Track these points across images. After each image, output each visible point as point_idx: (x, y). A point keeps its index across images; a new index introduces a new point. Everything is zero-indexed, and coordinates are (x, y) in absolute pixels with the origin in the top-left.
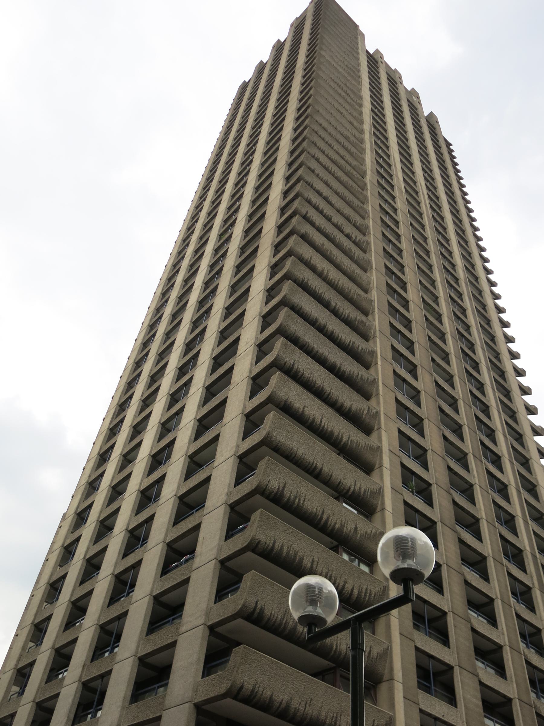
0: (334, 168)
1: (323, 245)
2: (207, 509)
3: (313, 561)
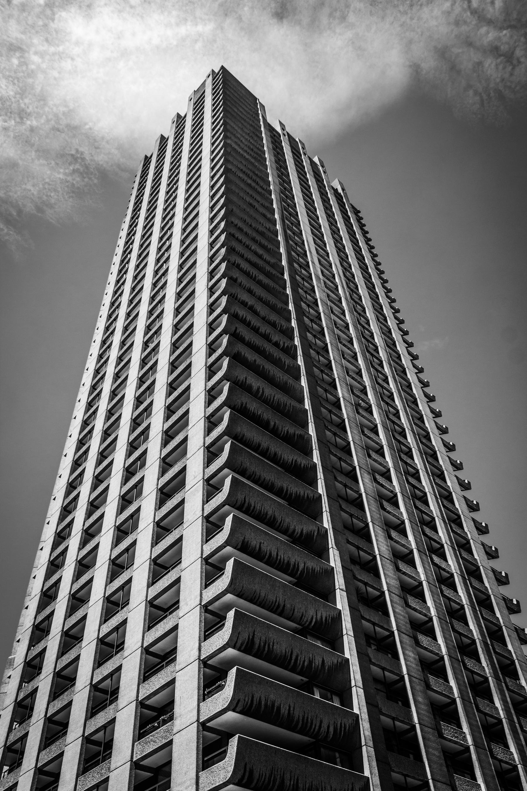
0: (254, 272)
1: (255, 361)
2: (179, 665)
3: (290, 707)
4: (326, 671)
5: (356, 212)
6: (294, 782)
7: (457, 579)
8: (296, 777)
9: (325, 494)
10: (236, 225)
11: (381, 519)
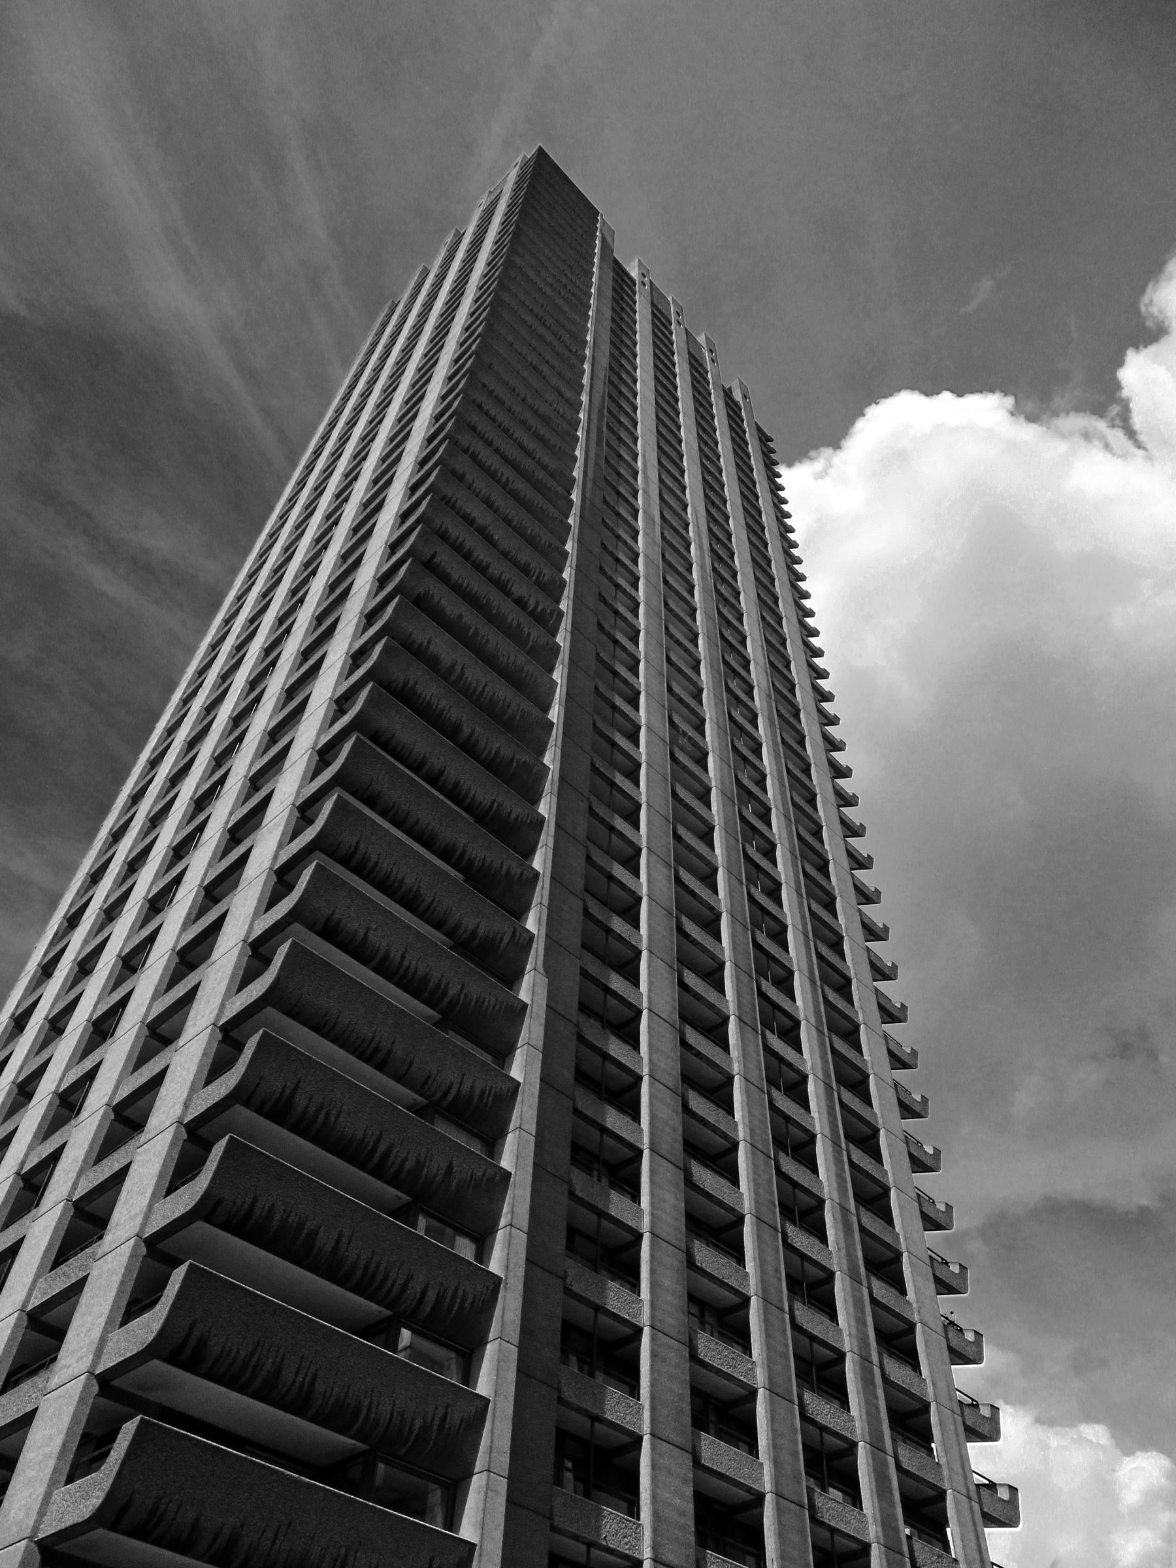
1: (460, 616)
4: (453, 1188)
5: (764, 439)
6: (304, 1378)
7: (813, 1089)
8: (312, 1370)
9: (548, 874)
10: (491, 392)
11: (672, 950)
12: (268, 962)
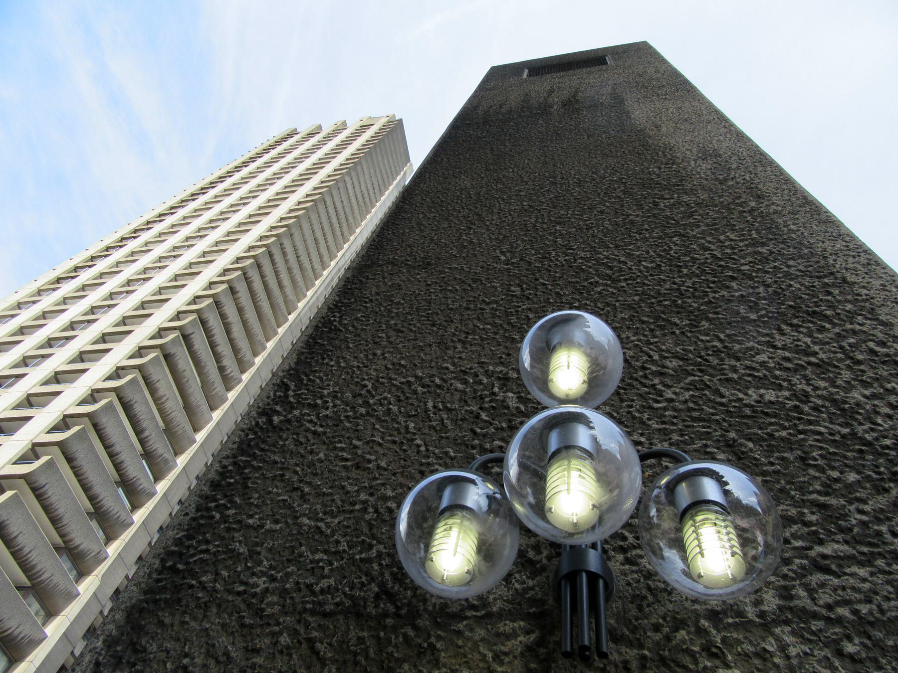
1: (185, 371)
12: (68, 428)
